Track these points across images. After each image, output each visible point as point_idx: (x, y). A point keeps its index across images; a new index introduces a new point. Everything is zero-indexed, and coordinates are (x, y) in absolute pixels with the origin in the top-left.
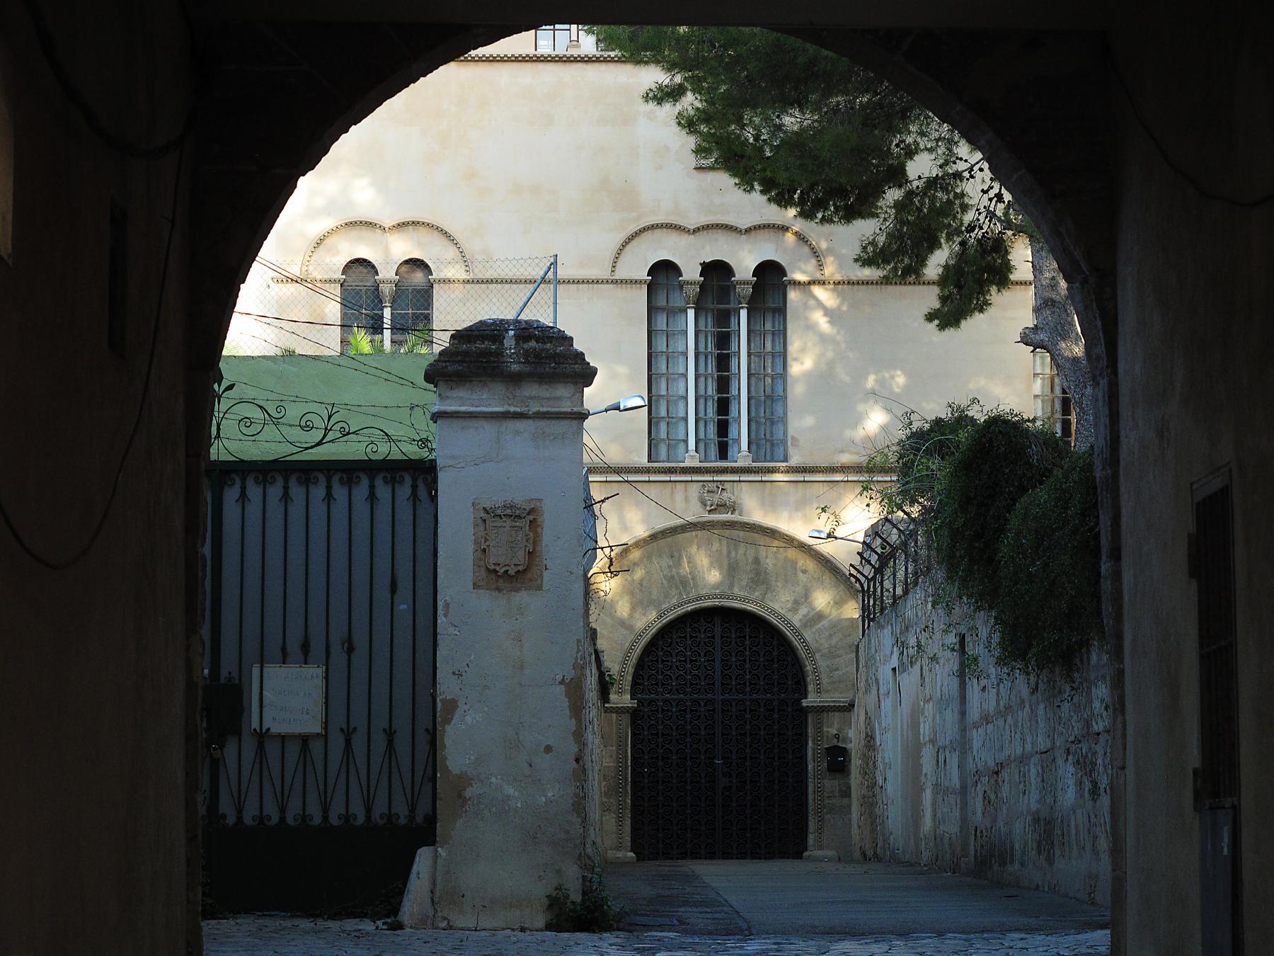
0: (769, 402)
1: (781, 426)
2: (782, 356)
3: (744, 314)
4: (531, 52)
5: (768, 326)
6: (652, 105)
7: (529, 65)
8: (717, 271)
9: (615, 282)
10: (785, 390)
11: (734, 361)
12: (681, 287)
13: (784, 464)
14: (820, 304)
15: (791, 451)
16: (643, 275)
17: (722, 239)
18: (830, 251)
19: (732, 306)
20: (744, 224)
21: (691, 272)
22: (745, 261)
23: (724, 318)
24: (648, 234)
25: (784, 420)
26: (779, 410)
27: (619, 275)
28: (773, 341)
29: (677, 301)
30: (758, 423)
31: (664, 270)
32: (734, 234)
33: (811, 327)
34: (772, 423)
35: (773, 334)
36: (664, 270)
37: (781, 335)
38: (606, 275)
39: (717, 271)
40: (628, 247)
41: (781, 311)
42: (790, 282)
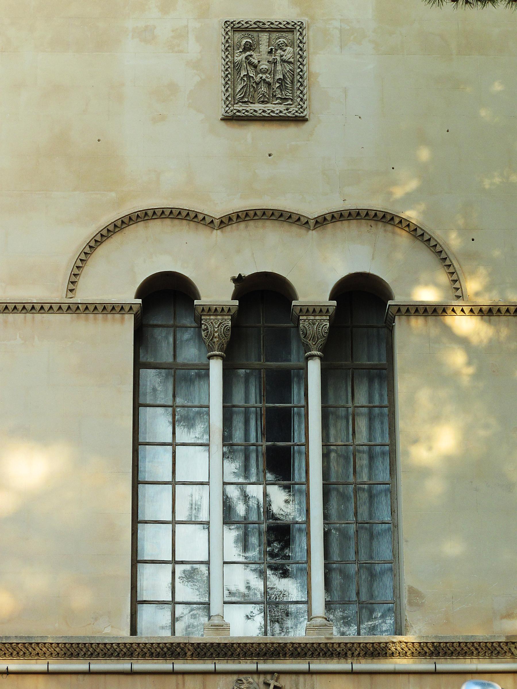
0: (364, 536)
1: (387, 580)
2: (387, 452)
3: (314, 369)
4: (123, 633)
5: (362, 398)
6: (223, 123)
7: (19, 317)
8: (264, 295)
9: (74, 309)
10: (394, 511)
11: (298, 464)
12: (198, 321)
13: (397, 638)
14: (464, 342)
15: (409, 614)
16: (128, 296)
17: (273, 235)
18: (472, 256)
19: (294, 361)
20: (312, 209)
21: (216, 291)
22: (315, 272)
23: (282, 384)
24: (138, 231)
25: (393, 566)
26: (383, 550)
27: (82, 296)
28: (371, 428)
29: (190, 353)
30: (346, 576)
31: (166, 296)
32: (295, 229)
33: (443, 378)
34: (373, 576)
35: (371, 419)
36: (166, 296)
37: (385, 414)
38: (57, 294)
39: (264, 295)
40: (101, 250)
41: (383, 375)
42: (399, 309)
